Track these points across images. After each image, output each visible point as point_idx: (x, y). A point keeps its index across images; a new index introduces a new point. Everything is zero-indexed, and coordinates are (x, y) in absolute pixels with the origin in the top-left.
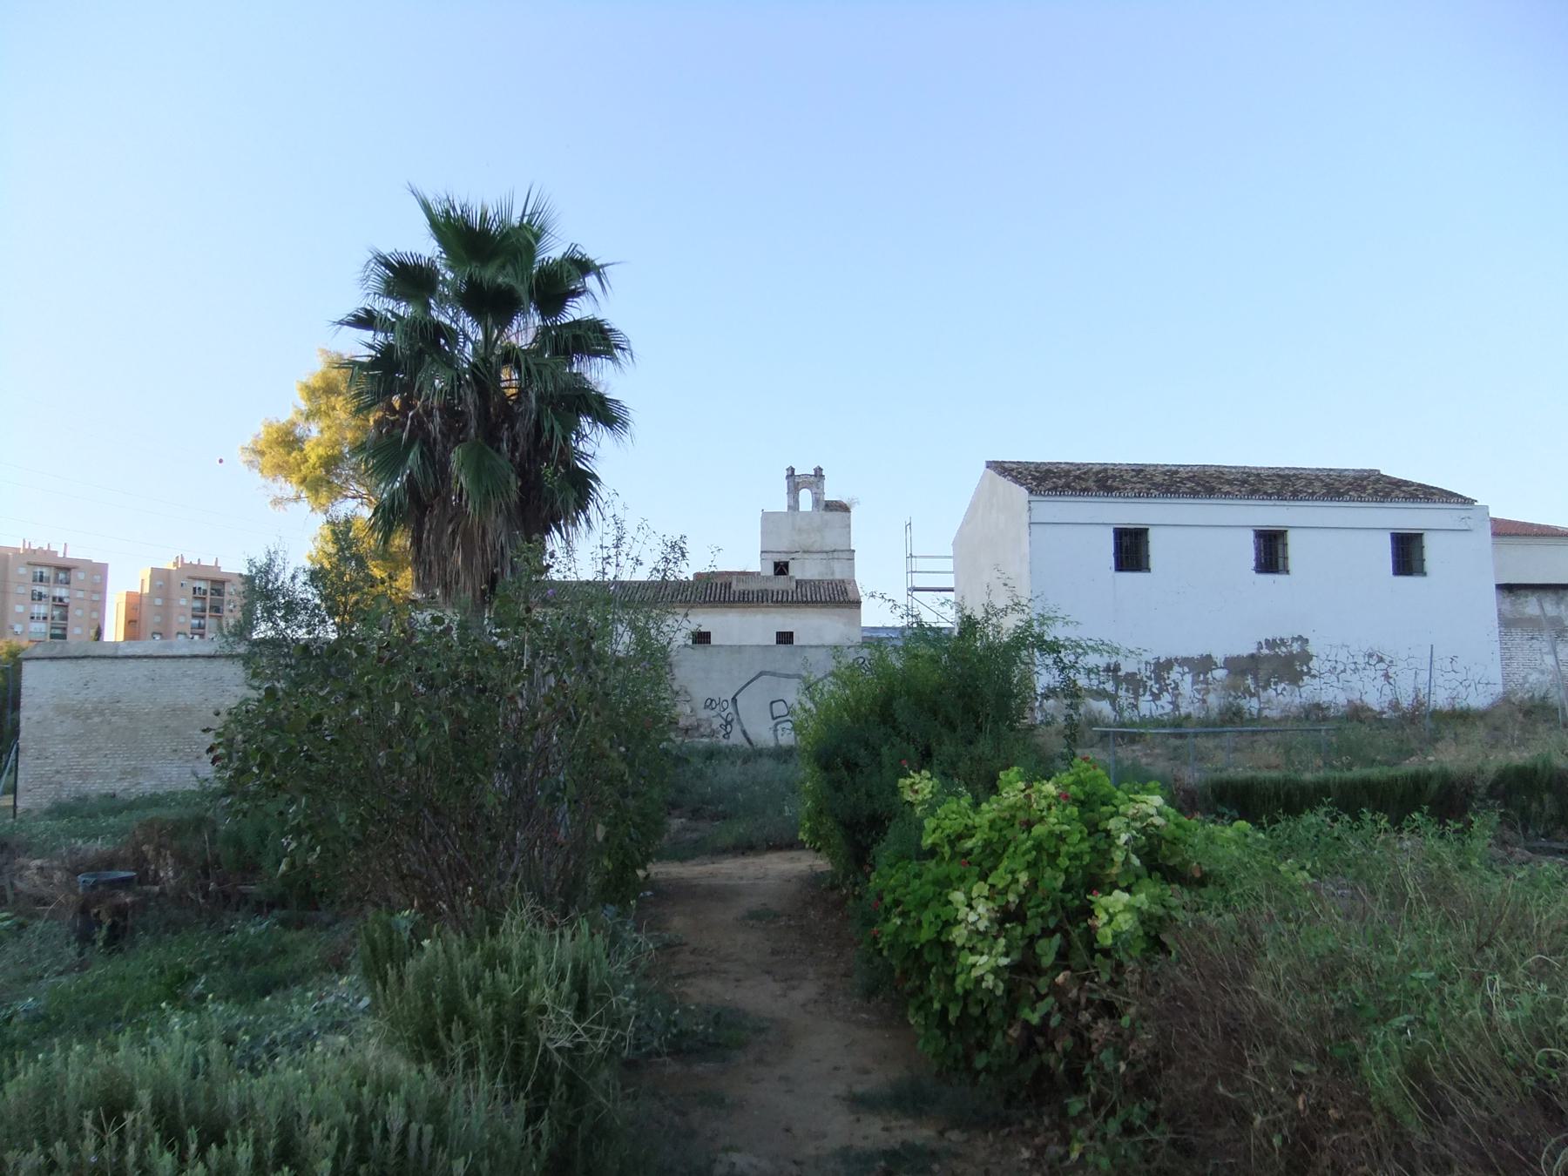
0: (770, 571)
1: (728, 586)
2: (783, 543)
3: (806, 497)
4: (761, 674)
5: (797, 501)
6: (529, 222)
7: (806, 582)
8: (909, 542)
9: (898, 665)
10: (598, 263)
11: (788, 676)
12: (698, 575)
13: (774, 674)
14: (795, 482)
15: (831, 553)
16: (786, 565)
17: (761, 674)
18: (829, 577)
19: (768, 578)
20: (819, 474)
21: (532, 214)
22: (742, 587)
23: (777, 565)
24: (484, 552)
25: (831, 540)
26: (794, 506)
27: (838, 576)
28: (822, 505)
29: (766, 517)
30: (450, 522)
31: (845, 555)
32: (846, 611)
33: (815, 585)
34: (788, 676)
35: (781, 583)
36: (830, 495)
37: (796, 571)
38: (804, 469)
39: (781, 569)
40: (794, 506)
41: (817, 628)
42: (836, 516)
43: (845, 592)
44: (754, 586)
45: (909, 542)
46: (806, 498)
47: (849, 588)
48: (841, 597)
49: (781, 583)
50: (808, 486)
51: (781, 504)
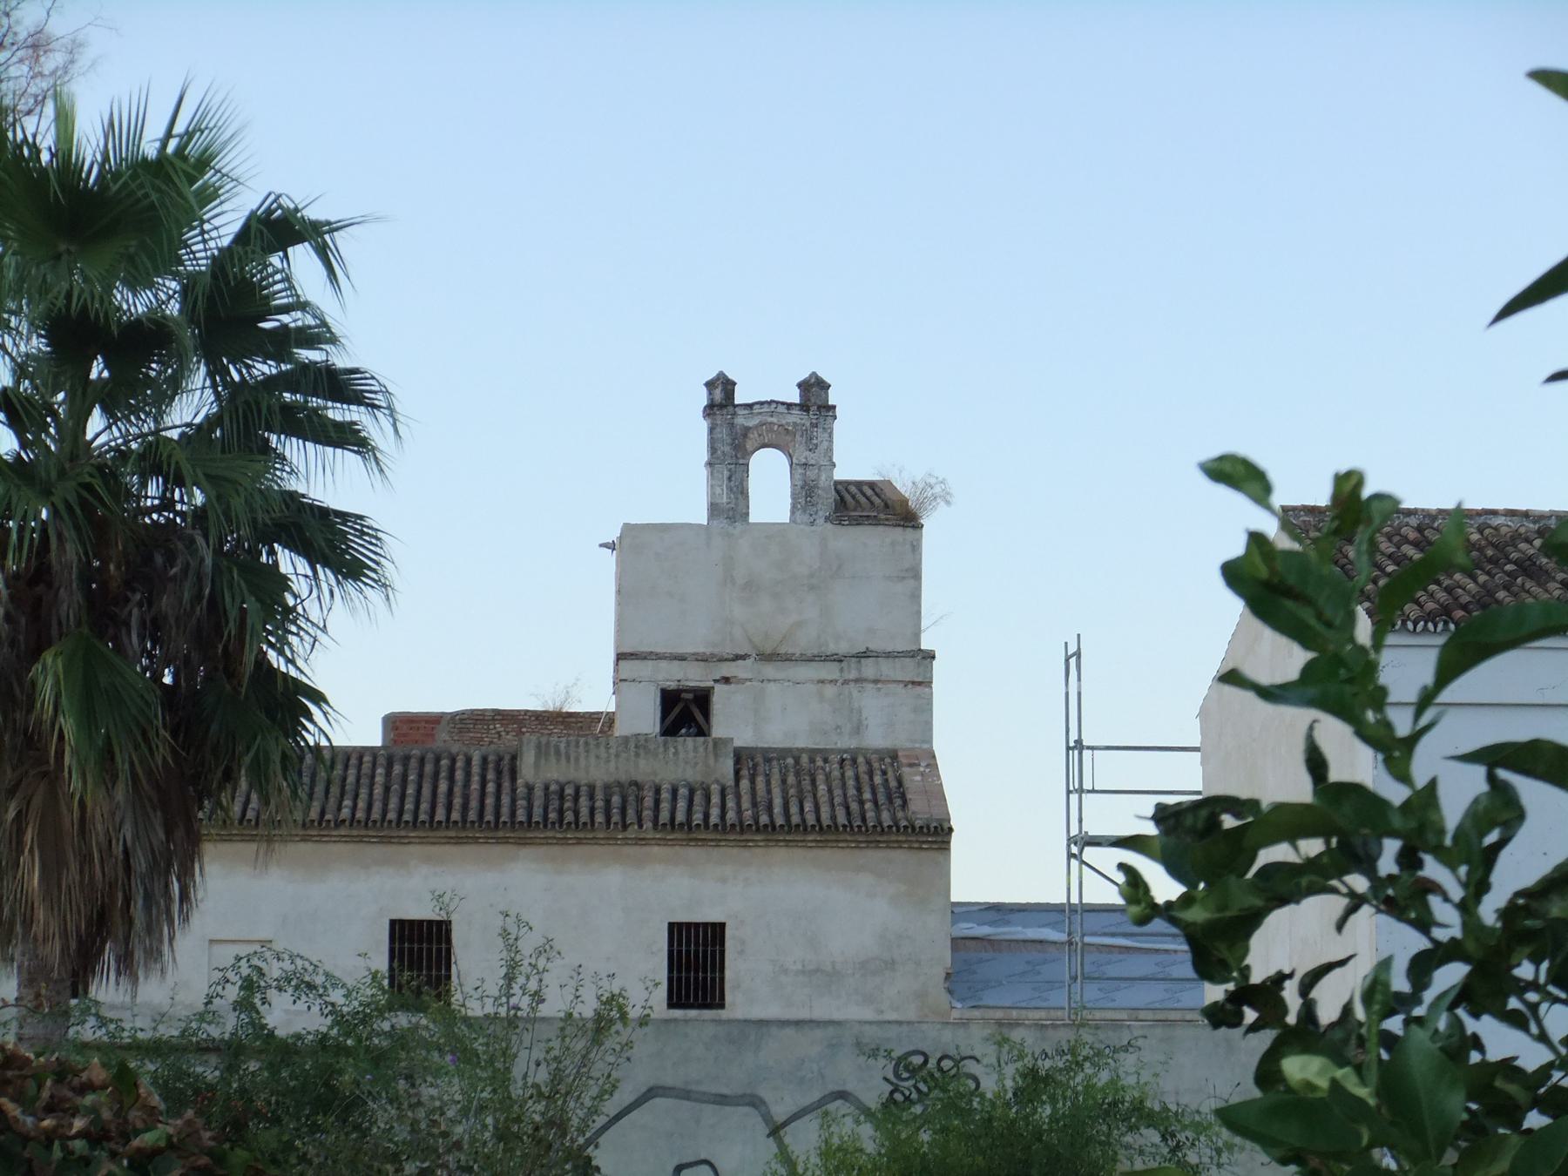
0: (645, 718)
1: (507, 767)
2: (693, 627)
3: (770, 482)
4: (651, 1093)
5: (739, 491)
6: (180, 151)
7: (768, 755)
8: (1073, 706)
9: (989, 1085)
10: (312, 214)
11: (722, 1100)
12: (398, 725)
13: (685, 1094)
14: (732, 423)
15: (853, 663)
16: (703, 699)
17: (651, 1093)
18: (846, 742)
19: (638, 744)
20: (814, 388)
21: (189, 135)
22: (555, 772)
23: (670, 699)
24: (85, 859)
25: (855, 618)
26: (730, 502)
27: (876, 738)
28: (827, 499)
29: (636, 546)
30: (11, 793)
31: (907, 670)
32: (900, 858)
33: (800, 767)
34: (722, 1100)
35: (683, 763)
36: (853, 459)
37: (734, 722)
38: (767, 382)
39: (685, 712)
40: (730, 502)
41: (794, 918)
42: (871, 541)
43: (898, 795)
44: (596, 769)
45: (1073, 706)
46: (770, 482)
47: (913, 779)
48: (883, 809)
49: (683, 763)
50: (778, 439)
51: (687, 499)
